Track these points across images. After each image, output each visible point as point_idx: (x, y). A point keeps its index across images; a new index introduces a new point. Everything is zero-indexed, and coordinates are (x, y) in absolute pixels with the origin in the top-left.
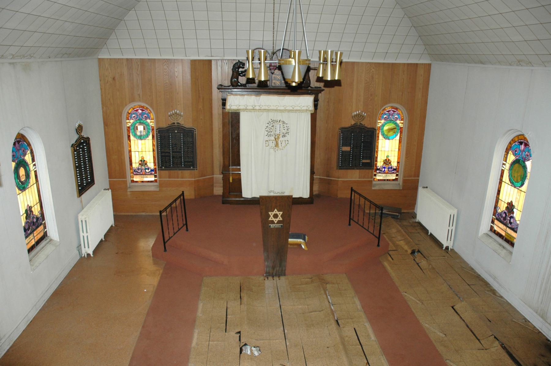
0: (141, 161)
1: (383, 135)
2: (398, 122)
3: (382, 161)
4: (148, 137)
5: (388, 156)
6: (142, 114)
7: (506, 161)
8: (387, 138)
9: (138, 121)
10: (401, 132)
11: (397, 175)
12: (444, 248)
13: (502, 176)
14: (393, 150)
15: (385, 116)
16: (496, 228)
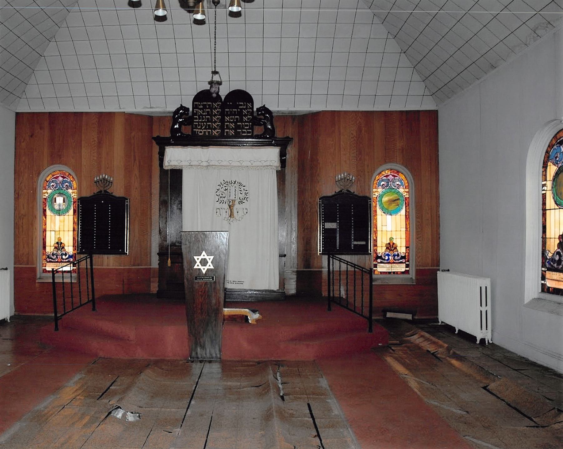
0: (57, 243)
1: (382, 208)
2: (401, 190)
3: (384, 245)
4: (68, 211)
5: (391, 239)
6: (63, 183)
7: (546, 180)
8: (387, 212)
9: (58, 192)
10: (407, 205)
11: (407, 266)
12: (478, 342)
13: (544, 204)
14: (399, 229)
15: (383, 183)
16: (549, 284)
